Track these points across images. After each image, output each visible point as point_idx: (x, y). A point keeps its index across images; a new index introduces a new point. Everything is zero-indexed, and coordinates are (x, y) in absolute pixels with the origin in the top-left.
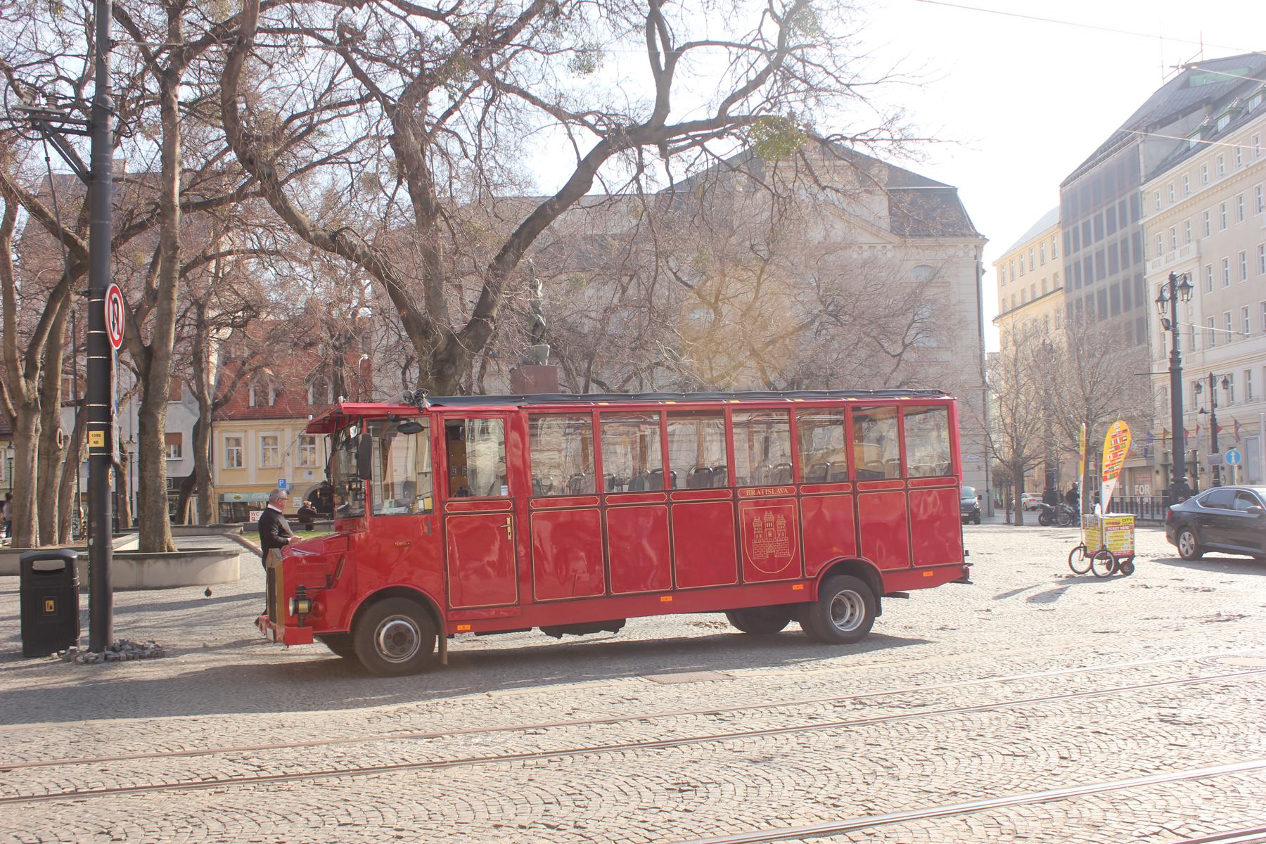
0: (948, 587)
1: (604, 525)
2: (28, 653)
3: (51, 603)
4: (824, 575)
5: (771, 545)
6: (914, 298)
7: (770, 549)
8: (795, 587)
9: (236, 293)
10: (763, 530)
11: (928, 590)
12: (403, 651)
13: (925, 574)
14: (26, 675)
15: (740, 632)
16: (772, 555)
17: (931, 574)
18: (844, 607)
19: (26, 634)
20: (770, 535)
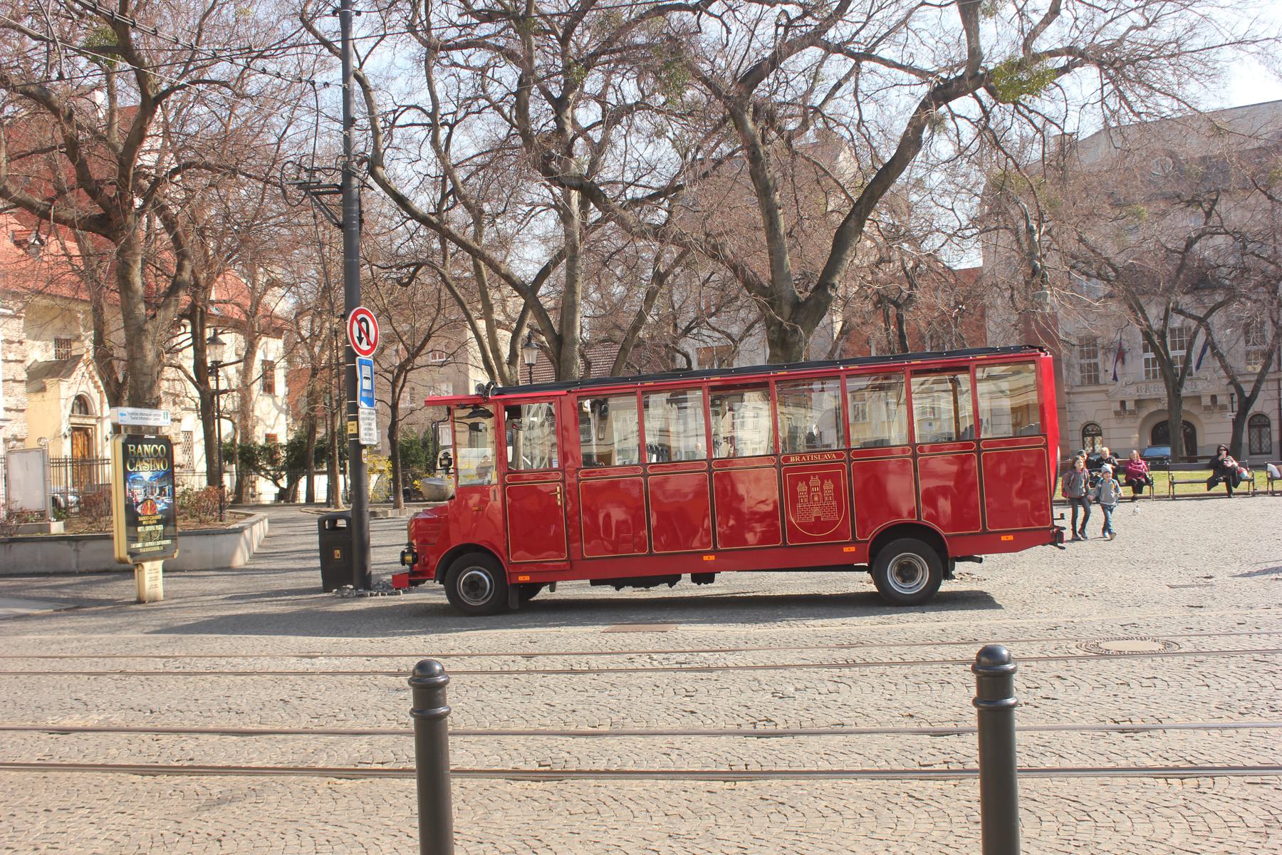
0: (1049, 547)
1: (647, 492)
2: (326, 588)
3: (338, 552)
4: (495, 556)
5: (817, 509)
6: (411, 58)
7: (816, 512)
8: (846, 550)
9: (552, 192)
10: (809, 494)
11: (995, 555)
12: (913, 578)
13: (1004, 538)
14: (281, 605)
15: (535, 598)
16: (818, 518)
17: (1011, 538)
18: (917, 571)
19: (325, 577)
20: (816, 499)
